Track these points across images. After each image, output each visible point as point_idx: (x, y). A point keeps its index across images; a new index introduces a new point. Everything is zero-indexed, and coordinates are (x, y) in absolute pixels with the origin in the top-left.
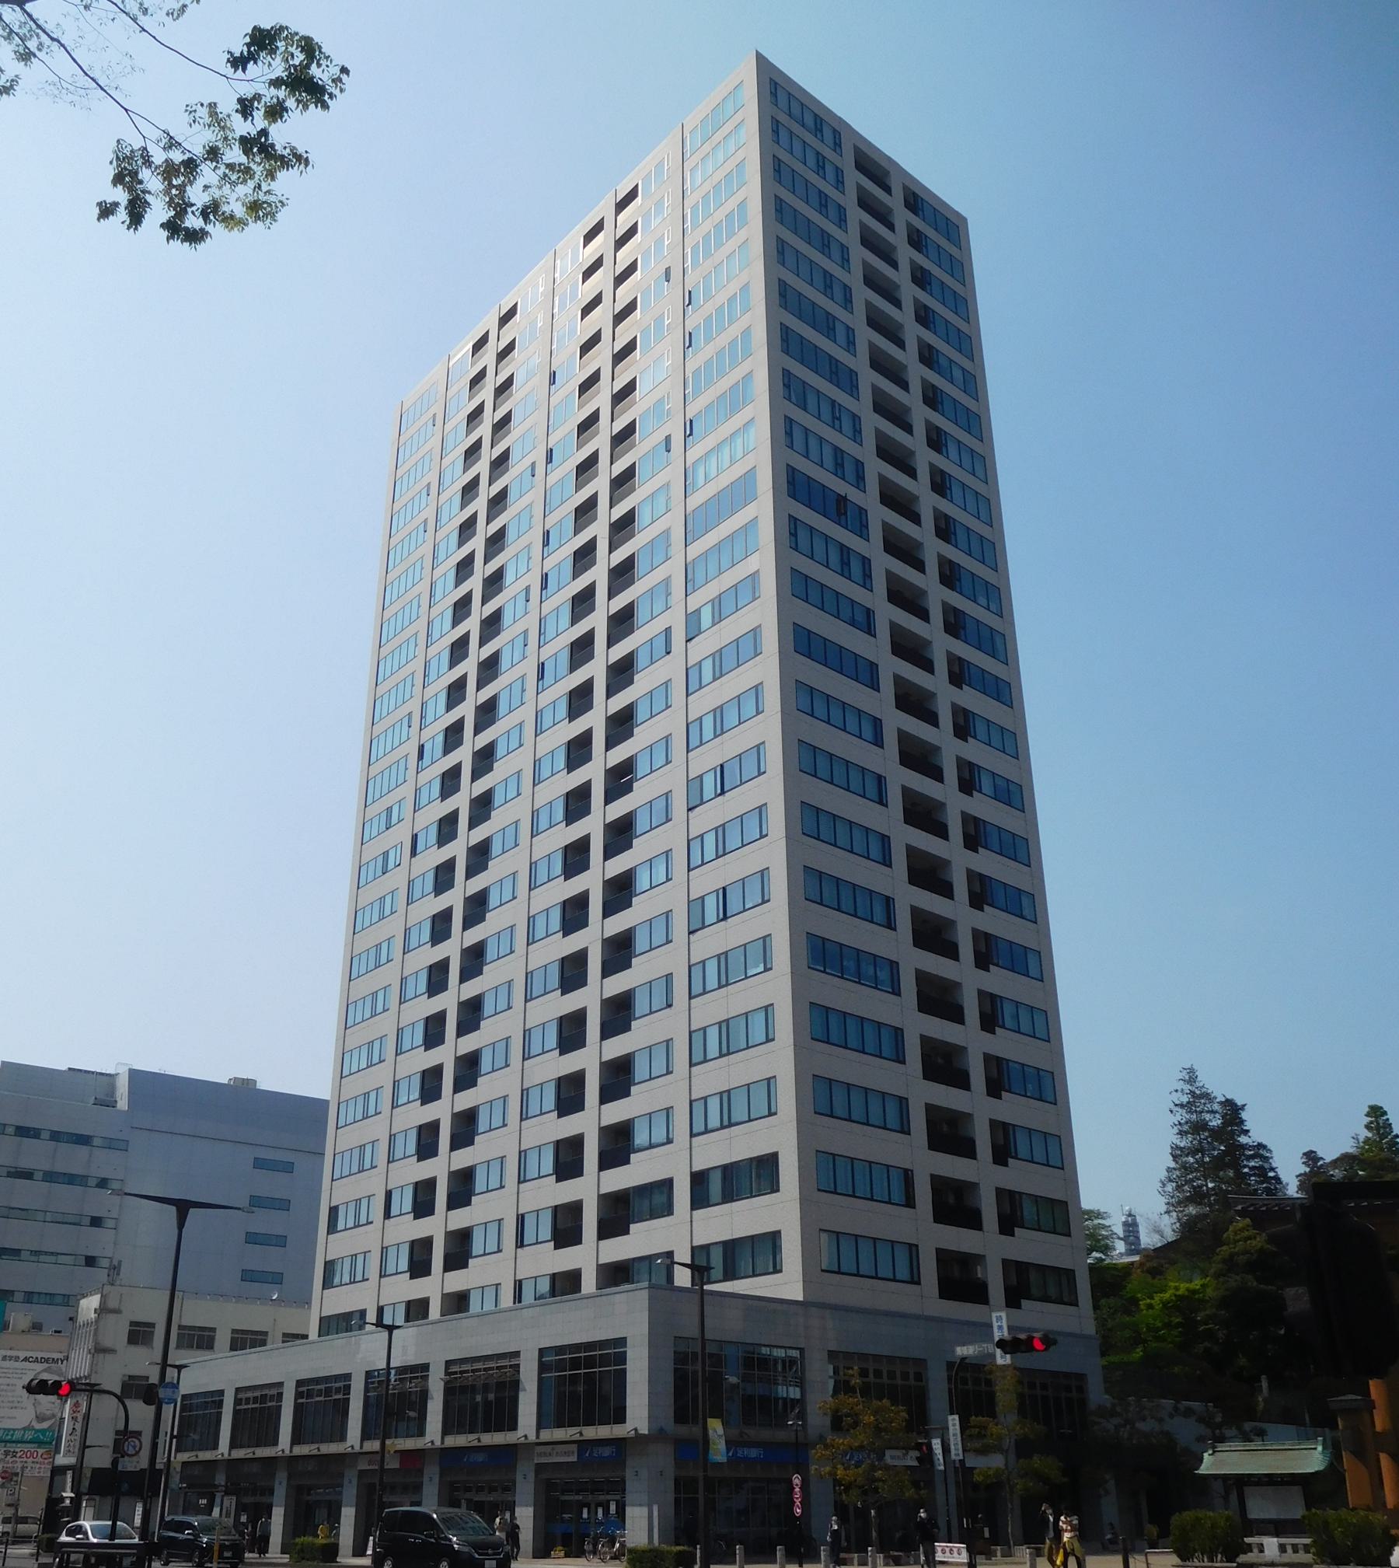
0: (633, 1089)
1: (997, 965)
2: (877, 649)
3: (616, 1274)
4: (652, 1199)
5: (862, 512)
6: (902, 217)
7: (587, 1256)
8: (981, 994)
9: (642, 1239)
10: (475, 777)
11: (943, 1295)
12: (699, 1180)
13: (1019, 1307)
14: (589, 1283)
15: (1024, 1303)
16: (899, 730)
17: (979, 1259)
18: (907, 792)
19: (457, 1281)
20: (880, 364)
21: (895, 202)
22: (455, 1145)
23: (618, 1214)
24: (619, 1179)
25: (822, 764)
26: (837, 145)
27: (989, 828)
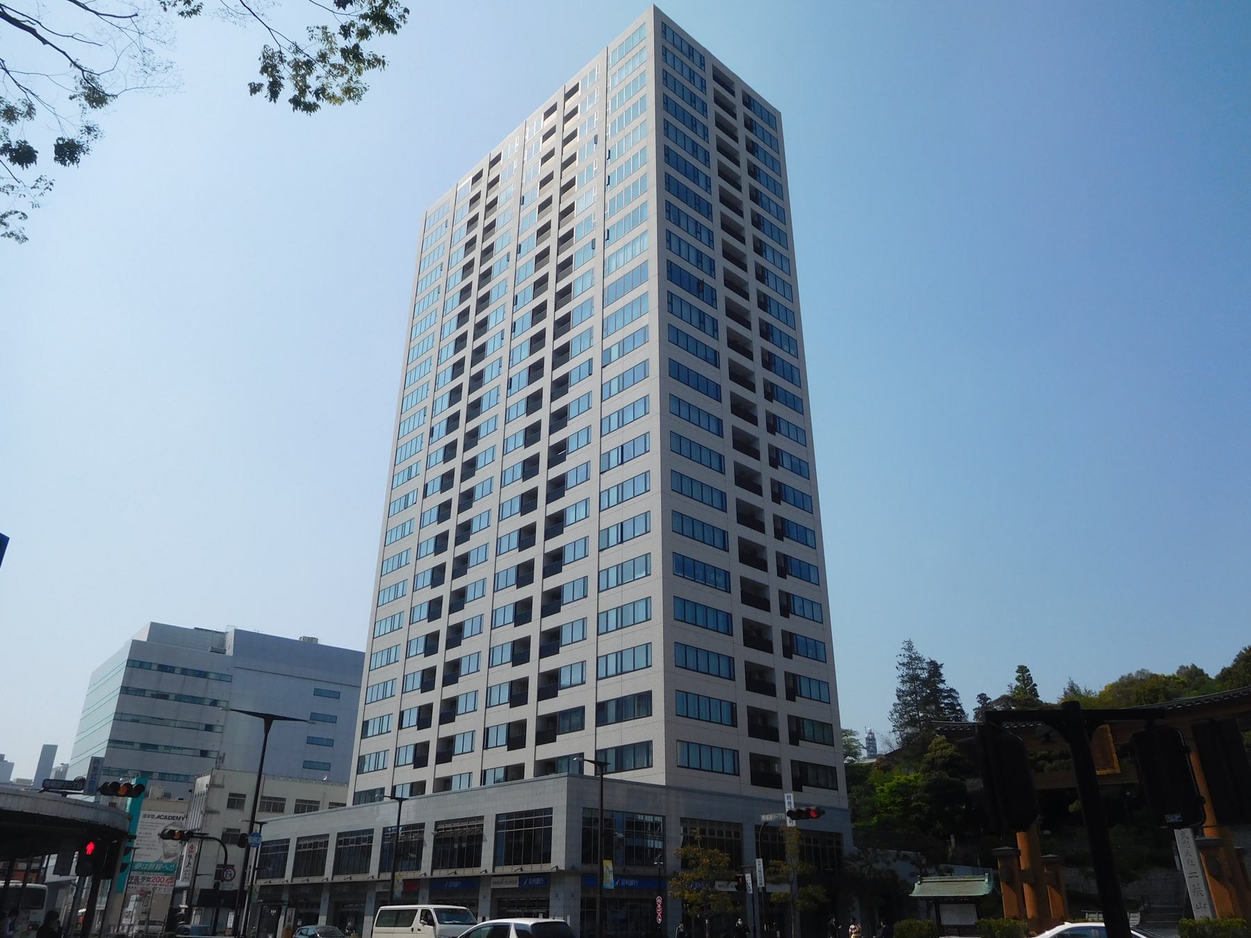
2: (720, 376)
3: (547, 767)
4: (571, 720)
6: (741, 110)
7: (528, 755)
8: (784, 633)
9: (564, 745)
12: (601, 707)
13: (801, 790)
14: (529, 773)
19: (444, 770)
21: (737, 101)
23: (550, 728)
24: (550, 706)
25: (682, 340)
26: (702, 65)
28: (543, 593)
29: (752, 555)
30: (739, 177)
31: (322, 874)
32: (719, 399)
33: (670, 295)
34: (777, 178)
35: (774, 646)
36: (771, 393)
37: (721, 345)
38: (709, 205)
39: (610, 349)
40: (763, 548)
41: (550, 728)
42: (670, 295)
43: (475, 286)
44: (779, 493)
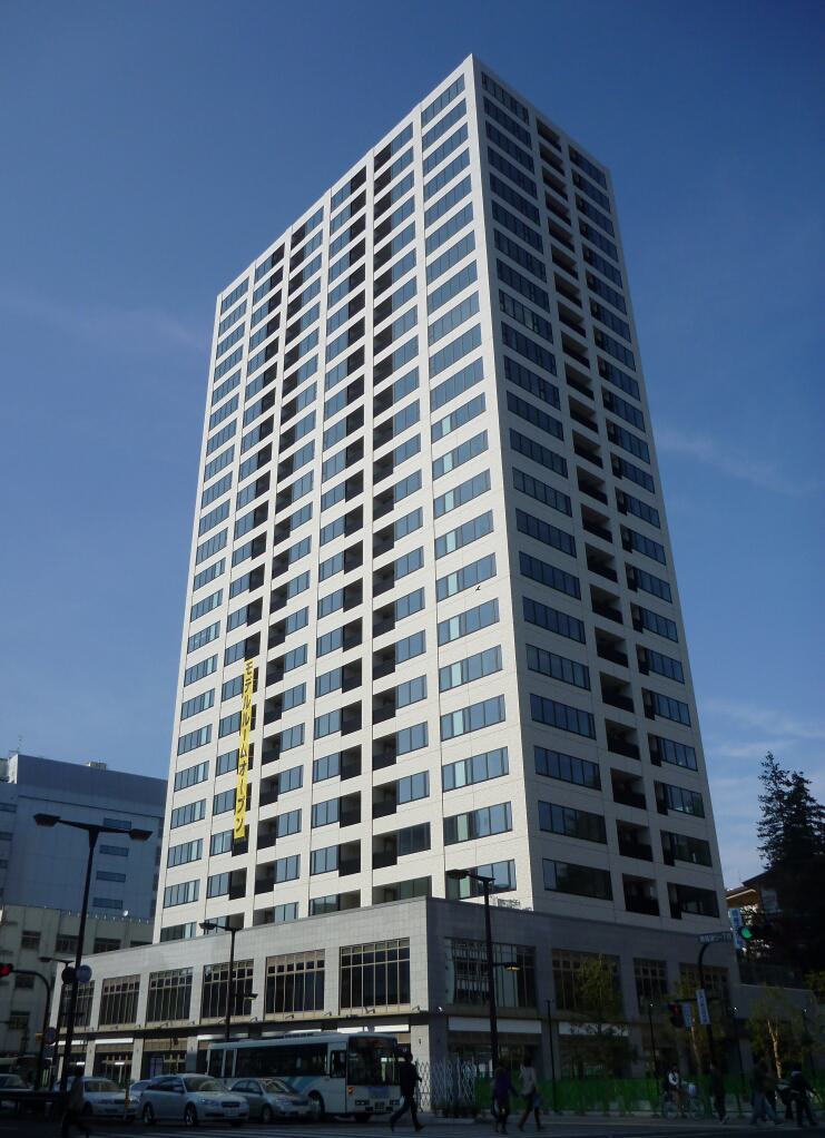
0: (398, 807)
1: (686, 911)
2: (573, 525)
3: (387, 894)
4: (417, 838)
5: (552, 357)
6: (568, 166)
7: (366, 880)
8: (663, 834)
9: (408, 867)
10: (275, 574)
11: (629, 909)
12: (450, 825)
13: (680, 918)
14: (366, 900)
15: (677, 862)
16: (582, 505)
17: (651, 882)
18: (589, 548)
19: (266, 901)
20: (562, 287)
21: (564, 156)
22: (265, 761)
23: (388, 849)
24: (388, 824)
25: (529, 485)
26: (526, 118)
27: (674, 791)
28: (374, 742)
29: (615, 693)
30: (567, 210)
31: (134, 1020)
32: (573, 553)
33: (502, 294)
34: (618, 290)
35: (648, 802)
36: (620, 469)
37: (563, 415)
38: (545, 295)
39: (445, 536)
40: (621, 641)
41: (388, 849)
42: (502, 294)
43: (277, 420)
44: (641, 620)
